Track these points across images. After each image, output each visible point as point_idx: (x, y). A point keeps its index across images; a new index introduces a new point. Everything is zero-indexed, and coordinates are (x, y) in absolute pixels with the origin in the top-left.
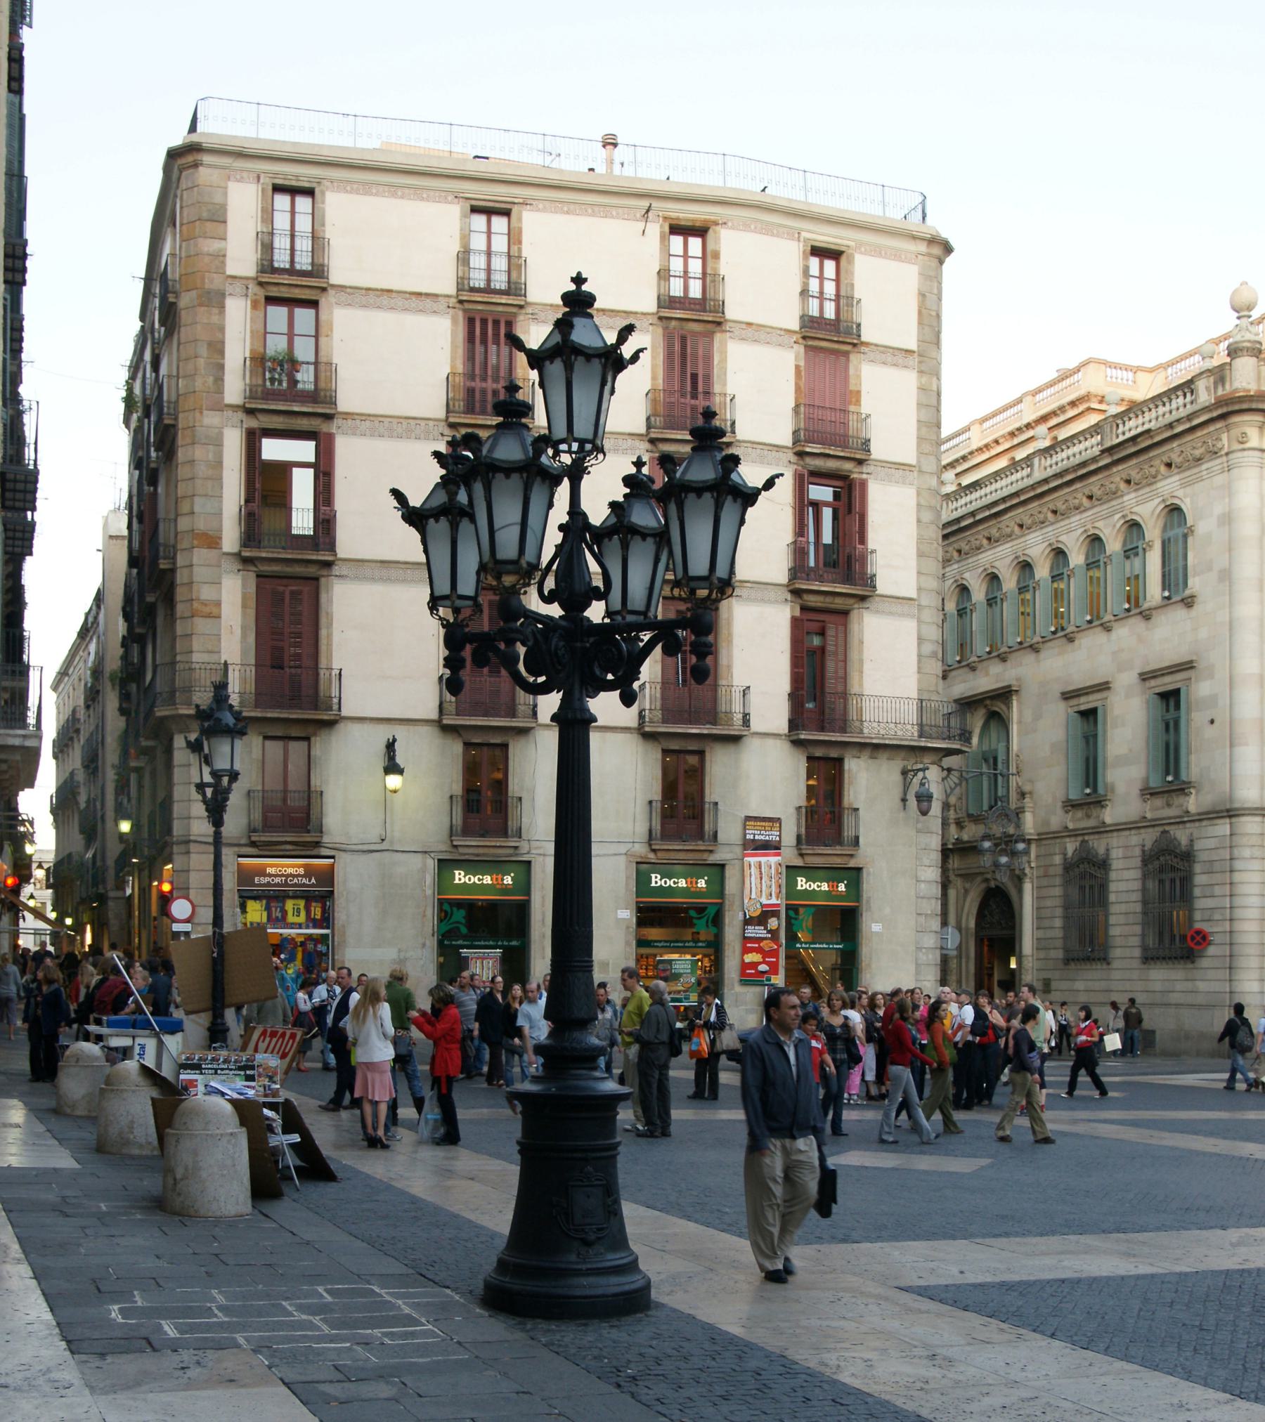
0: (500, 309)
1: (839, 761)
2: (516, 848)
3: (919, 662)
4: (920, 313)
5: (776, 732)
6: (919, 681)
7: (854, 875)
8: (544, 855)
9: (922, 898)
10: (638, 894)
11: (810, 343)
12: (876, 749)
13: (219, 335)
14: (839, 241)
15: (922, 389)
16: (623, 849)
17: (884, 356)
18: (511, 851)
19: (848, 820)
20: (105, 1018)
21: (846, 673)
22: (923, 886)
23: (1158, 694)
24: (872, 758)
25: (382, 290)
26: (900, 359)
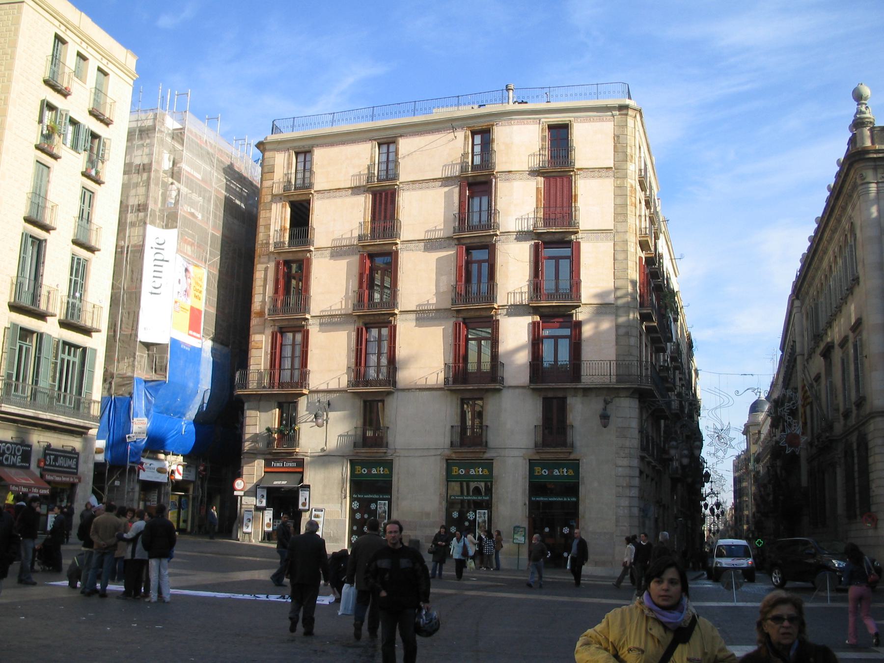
0: (387, 188)
1: (564, 400)
2: (385, 453)
3: (617, 339)
4: (615, 147)
5: (522, 385)
6: (617, 350)
7: (575, 465)
8: (399, 456)
9: (620, 476)
10: (530, 478)
11: (545, 175)
12: (587, 391)
13: (269, 222)
14: (564, 119)
15: (617, 187)
16: (439, 452)
17: (593, 173)
18: (382, 455)
19: (569, 432)
20: (292, 536)
21: (143, 242)
22: (620, 469)
23: (85, 84)
24: (584, 396)
25: (336, 189)
26: (604, 173)
